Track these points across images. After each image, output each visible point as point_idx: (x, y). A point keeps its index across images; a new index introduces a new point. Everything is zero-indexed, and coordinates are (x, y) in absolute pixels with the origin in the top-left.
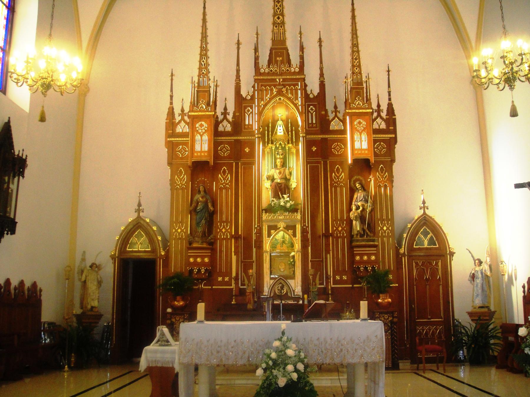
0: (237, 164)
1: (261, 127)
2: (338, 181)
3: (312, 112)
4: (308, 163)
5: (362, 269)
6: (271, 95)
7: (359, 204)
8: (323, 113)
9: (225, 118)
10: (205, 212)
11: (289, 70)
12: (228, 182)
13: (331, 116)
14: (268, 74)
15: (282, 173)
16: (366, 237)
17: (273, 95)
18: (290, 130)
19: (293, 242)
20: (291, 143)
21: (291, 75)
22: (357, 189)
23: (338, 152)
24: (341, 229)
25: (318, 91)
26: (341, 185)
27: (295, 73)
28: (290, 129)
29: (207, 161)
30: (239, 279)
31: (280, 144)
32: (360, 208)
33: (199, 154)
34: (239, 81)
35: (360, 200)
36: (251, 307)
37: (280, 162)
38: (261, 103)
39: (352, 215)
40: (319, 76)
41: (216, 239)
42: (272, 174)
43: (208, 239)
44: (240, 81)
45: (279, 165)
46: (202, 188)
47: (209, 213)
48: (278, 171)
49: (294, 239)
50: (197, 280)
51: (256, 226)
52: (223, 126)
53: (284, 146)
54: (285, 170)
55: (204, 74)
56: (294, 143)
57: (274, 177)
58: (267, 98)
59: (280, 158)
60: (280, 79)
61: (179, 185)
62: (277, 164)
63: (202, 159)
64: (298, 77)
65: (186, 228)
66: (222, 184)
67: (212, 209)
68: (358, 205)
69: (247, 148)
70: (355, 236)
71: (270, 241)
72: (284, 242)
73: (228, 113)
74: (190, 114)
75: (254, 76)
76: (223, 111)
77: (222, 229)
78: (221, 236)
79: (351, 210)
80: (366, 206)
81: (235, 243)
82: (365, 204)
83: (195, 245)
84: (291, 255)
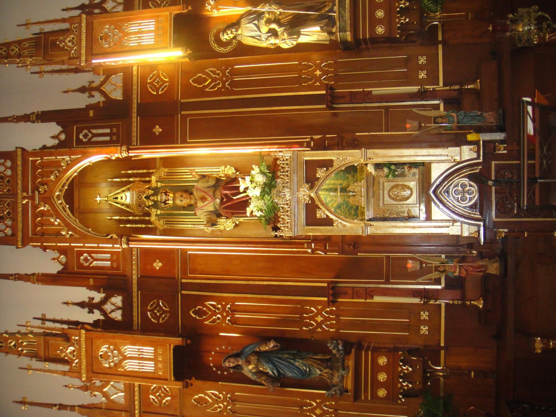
0: (186, 286)
1: (109, 237)
2: (220, 79)
3: (90, 135)
4: (184, 141)
5: (404, 4)
6: (52, 216)
7: (265, 29)
8: (91, 113)
9: (99, 306)
10: (280, 358)
11: (9, 180)
12: (219, 306)
13: (98, 98)
14: (14, 220)
15: (203, 194)
16: (335, 12)
17: (51, 211)
18: (127, 179)
19: (343, 168)
20: (150, 177)
21: (17, 175)
22: (235, 38)
23: (165, 82)
24: (318, 71)
25: (54, 124)
26: (228, 73)
27: (13, 168)
28: (124, 180)
29: (173, 350)
30: (425, 289)
31: (147, 198)
32: (274, 29)
33: (160, 366)
34: (35, 277)
35: (256, 29)
36: (496, 265)
37: (182, 199)
38: (64, 235)
39: (286, 43)
40: (29, 123)
41: (336, 338)
42: (206, 215)
43: (337, 356)
44: (34, 274)
45: (188, 200)
46: (229, 362)
47: (282, 350)
48: (200, 204)
49: (336, 165)
50: (425, 379)
51: (309, 251)
52: (113, 311)
53: (152, 189)
54: (198, 189)
55: (16, 344)
56: (151, 171)
57: (211, 212)
58: (56, 223)
59: (174, 200)
60: (23, 196)
61: (226, 407)
62: (186, 205)
63: (170, 359)
64: (19, 163)
65: (313, 397)
66: (224, 318)
67: (272, 344)
68: (267, 33)
69: (155, 265)
70: (333, 38)
71: (340, 221)
72: (344, 190)
73: (89, 301)
74: (84, 379)
75: (18, 248)
76: (87, 310)
77: (316, 321)
78: (331, 326)
79: (278, 50)
80: (269, 15)
81: (345, 294)
82: (265, 19)
83: (349, 385)
84: (373, 173)
